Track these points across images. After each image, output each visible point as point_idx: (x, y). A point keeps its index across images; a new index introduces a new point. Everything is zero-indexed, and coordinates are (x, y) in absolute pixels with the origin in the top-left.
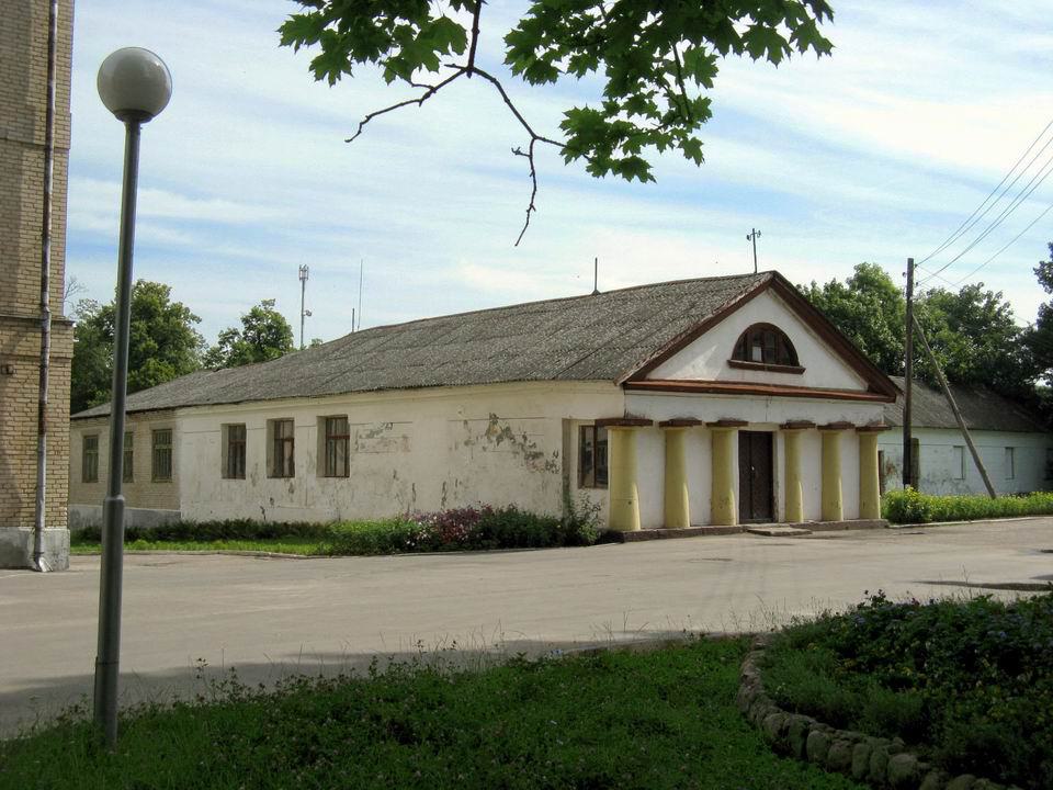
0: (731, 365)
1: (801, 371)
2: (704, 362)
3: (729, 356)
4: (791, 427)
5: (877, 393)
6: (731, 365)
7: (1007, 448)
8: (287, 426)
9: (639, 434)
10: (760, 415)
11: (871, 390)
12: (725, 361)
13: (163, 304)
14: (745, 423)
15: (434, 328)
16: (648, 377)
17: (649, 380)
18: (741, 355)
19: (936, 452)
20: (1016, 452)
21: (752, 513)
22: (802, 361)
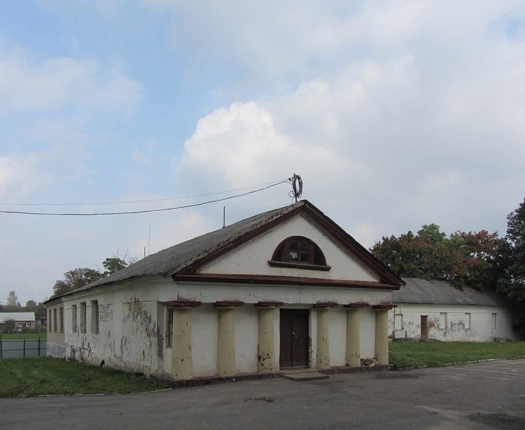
0: (271, 264)
1: (328, 269)
2: (256, 259)
3: (270, 258)
4: (321, 308)
5: (385, 283)
6: (271, 264)
7: (492, 314)
8: (83, 331)
9: (327, 317)
10: (292, 298)
11: (382, 281)
12: (267, 262)
13: (503, 246)
14: (282, 304)
15: (207, 235)
16: (197, 272)
17: (199, 274)
18: (280, 257)
19: (455, 316)
20: (497, 315)
21: (292, 362)
22: (329, 262)
